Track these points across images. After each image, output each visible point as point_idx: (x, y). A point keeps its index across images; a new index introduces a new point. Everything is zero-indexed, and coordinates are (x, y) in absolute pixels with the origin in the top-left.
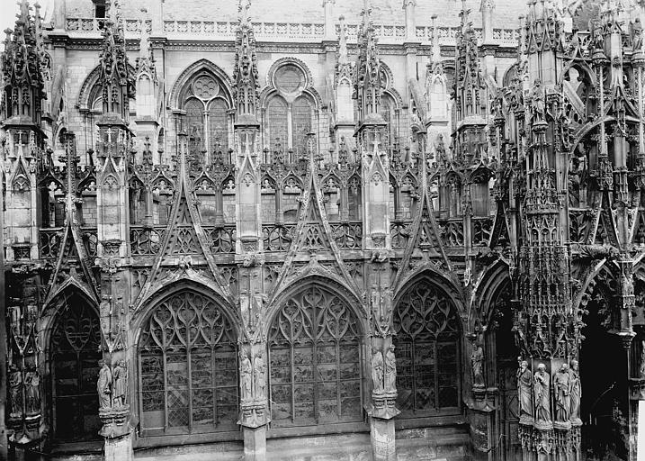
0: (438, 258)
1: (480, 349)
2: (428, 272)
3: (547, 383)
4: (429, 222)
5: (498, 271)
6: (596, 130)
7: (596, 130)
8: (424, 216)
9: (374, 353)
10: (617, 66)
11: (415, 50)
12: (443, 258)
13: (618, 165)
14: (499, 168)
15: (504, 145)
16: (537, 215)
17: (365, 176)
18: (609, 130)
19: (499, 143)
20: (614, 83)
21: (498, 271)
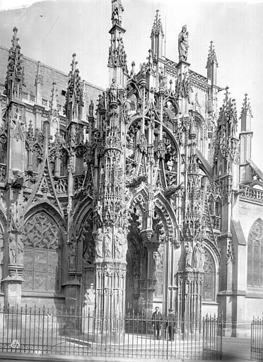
0: (52, 198)
1: (74, 250)
2: (45, 204)
3: (111, 237)
4: (48, 176)
5: (86, 204)
6: (140, 120)
7: (140, 120)
8: (45, 172)
9: (11, 241)
10: (152, 92)
11: (41, 112)
12: (55, 199)
13: (150, 143)
14: (90, 145)
15: (93, 132)
16: (110, 149)
17: (12, 133)
18: (146, 124)
19: (90, 131)
20: (150, 101)
21: (86, 204)
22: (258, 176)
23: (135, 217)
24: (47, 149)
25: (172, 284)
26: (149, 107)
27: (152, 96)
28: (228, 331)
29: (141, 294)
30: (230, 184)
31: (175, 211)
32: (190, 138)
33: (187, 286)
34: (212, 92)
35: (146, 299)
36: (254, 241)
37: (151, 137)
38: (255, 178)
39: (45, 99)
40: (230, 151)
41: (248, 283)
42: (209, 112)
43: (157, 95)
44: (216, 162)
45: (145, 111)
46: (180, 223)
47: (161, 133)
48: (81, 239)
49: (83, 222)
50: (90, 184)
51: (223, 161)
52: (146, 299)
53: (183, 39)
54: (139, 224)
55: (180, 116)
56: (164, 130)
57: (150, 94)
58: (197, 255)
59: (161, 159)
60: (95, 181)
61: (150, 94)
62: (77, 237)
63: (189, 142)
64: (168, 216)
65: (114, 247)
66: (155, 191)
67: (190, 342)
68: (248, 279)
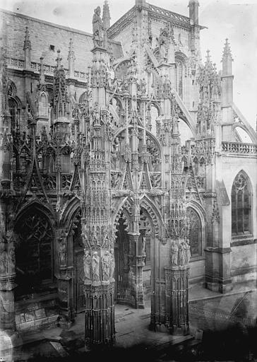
13: (134, 150)
18: (130, 132)
19: (76, 133)
22: (239, 119)
23: (121, 221)
24: (34, 149)
25: (159, 278)
26: (132, 116)
27: (134, 104)
28: (215, 286)
29: (131, 268)
30: (213, 146)
31: (161, 209)
32: (173, 136)
33: (174, 283)
34: (194, 30)
35: (135, 274)
36: (237, 192)
37: (136, 142)
38: (237, 120)
39: (34, 61)
40: (212, 114)
41: (232, 232)
42: (192, 51)
43: (139, 102)
44: (200, 122)
45: (128, 120)
46: (166, 222)
47: (145, 138)
48: (71, 234)
49: (72, 218)
50: (77, 185)
51: (206, 122)
52: (135, 274)
53: (163, 42)
54: (126, 226)
55: (163, 118)
56: (147, 134)
57: (133, 101)
58: (183, 254)
59: (145, 163)
60: (82, 182)
61: (133, 101)
62: (67, 234)
63: (172, 140)
64: (153, 214)
65: (101, 270)
66: (140, 194)
67: (181, 209)
68: (232, 228)
